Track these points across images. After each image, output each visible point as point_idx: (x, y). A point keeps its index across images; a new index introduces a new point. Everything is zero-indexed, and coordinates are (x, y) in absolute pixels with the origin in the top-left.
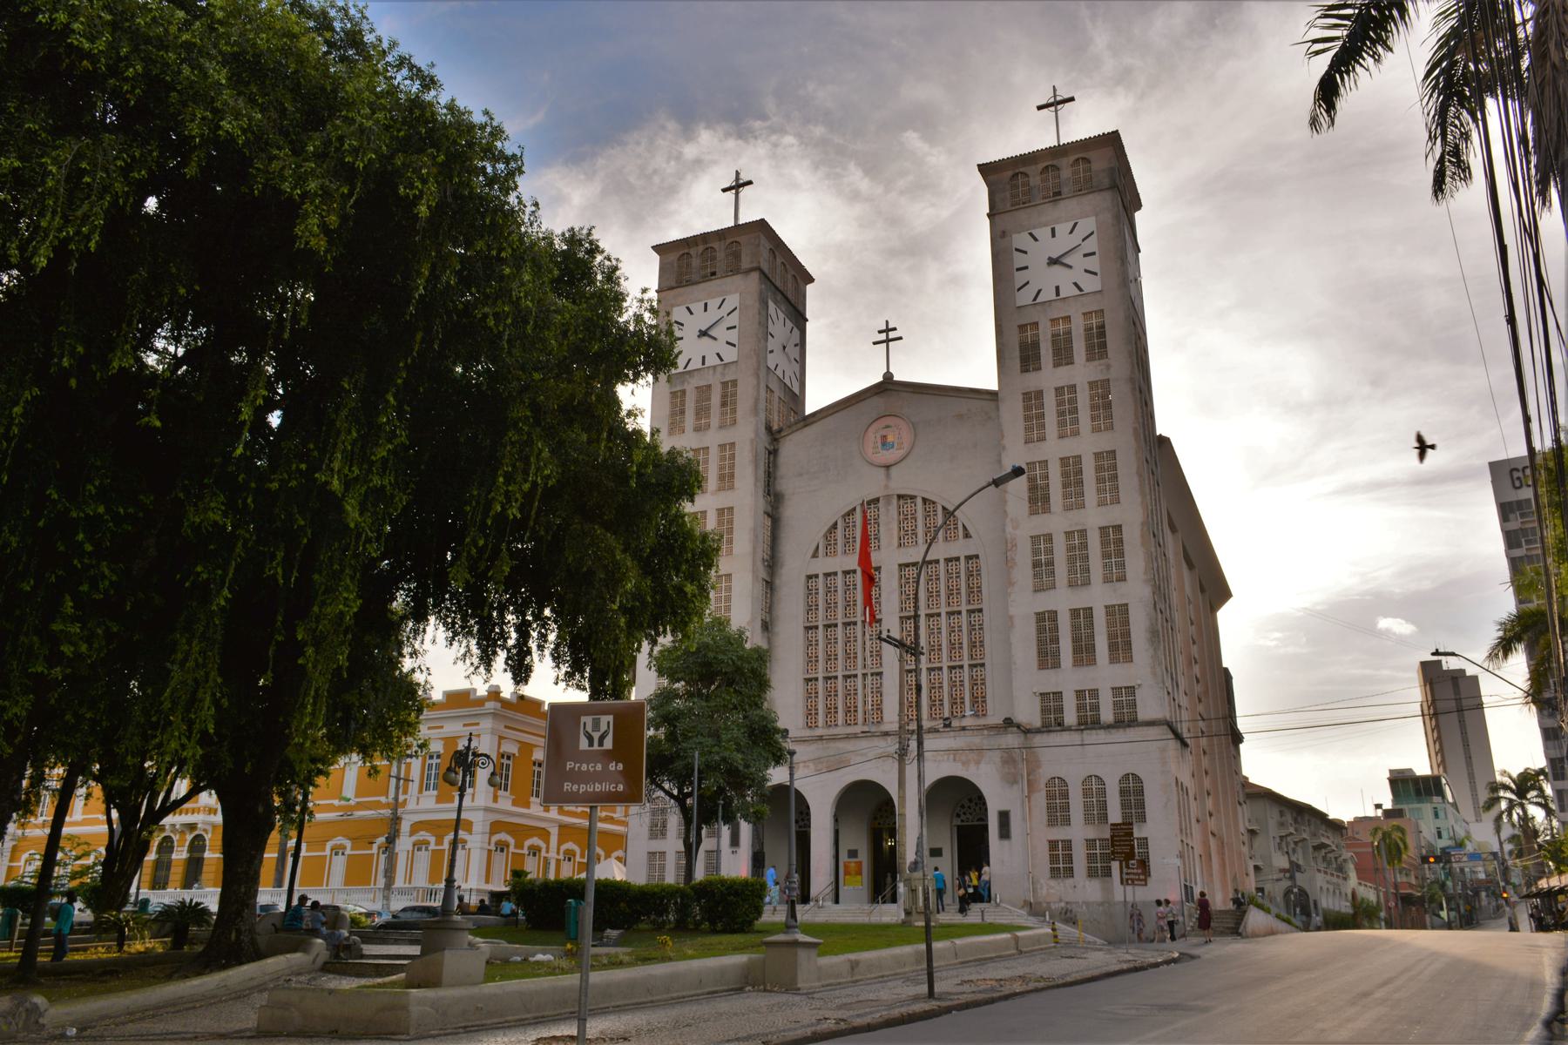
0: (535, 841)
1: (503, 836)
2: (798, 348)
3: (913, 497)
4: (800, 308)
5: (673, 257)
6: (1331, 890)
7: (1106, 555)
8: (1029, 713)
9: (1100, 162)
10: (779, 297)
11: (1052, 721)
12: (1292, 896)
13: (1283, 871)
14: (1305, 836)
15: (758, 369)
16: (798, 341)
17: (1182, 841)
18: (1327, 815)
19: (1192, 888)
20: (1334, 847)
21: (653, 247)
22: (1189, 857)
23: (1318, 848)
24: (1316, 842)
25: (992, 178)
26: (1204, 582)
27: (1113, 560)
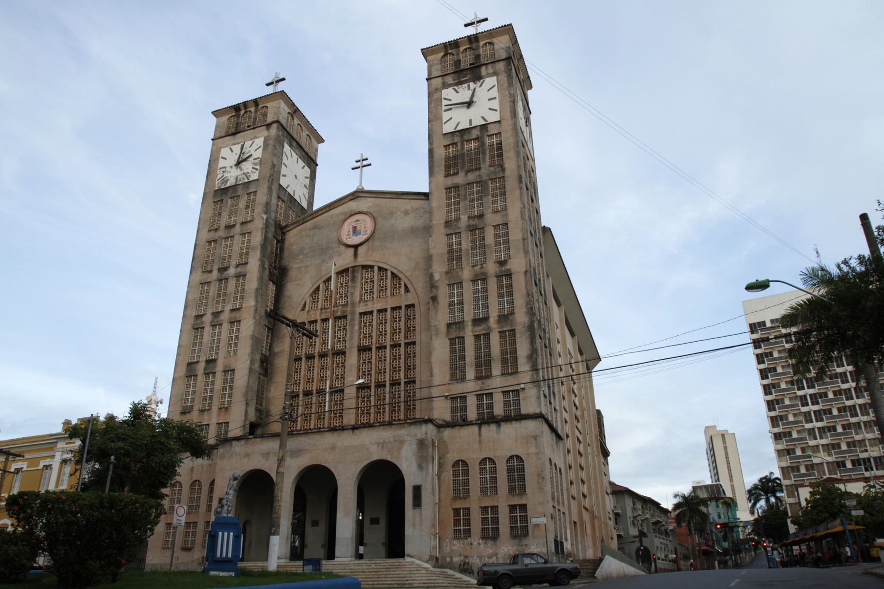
3: (372, 267)
6: (663, 548)
7: (501, 296)
8: (442, 410)
9: (501, 43)
11: (460, 422)
12: (640, 552)
13: (635, 537)
14: (648, 516)
15: (272, 184)
16: (309, 175)
17: (554, 507)
18: (660, 504)
19: (562, 543)
20: (664, 523)
22: (560, 520)
23: (655, 524)
24: (654, 520)
26: (568, 316)
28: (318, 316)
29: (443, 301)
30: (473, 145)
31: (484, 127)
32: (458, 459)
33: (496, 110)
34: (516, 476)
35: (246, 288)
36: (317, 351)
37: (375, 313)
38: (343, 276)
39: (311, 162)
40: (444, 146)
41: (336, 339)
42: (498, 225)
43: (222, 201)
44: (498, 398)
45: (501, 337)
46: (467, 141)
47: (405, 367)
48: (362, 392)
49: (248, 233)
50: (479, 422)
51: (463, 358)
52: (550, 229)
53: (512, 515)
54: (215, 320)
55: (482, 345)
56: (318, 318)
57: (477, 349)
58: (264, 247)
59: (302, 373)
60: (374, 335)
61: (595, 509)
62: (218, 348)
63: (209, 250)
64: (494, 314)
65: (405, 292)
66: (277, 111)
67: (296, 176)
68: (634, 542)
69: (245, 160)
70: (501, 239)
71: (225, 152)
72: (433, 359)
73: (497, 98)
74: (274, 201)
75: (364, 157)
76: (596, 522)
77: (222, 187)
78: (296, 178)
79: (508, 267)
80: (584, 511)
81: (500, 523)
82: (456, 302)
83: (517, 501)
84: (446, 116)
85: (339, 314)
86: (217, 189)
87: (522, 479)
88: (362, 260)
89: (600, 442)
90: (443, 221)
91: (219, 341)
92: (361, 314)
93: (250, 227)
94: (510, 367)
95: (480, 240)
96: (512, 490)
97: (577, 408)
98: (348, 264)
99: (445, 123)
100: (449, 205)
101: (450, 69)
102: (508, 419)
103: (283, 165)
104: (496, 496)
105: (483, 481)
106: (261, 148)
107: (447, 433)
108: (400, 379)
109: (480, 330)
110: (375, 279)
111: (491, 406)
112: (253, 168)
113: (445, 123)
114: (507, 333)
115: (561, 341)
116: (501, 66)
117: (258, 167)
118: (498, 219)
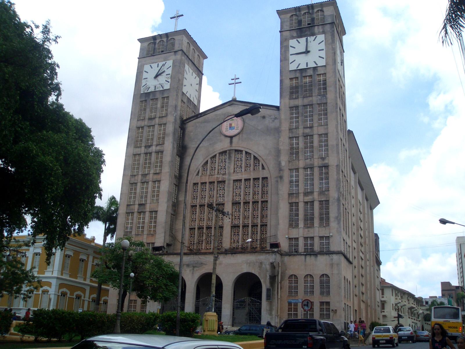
0: (79, 293)
1: (64, 290)
2: (198, 85)
3: (241, 151)
4: (200, 69)
5: (146, 44)
10: (190, 63)
11: (294, 252)
13: (395, 317)
16: (198, 83)
18: (415, 296)
21: (138, 40)
22: (348, 311)
25: (283, 16)
27: (324, 181)
28: (207, 179)
29: (286, 179)
30: (308, 80)
31: (315, 69)
32: (292, 274)
33: (323, 58)
34: (325, 286)
35: (163, 160)
36: (206, 201)
37: (243, 181)
38: (223, 155)
39: (200, 73)
40: (290, 79)
41: (218, 195)
42: (322, 134)
43: (146, 101)
44: (317, 241)
45: (320, 204)
46: (304, 77)
47: (261, 216)
48: (234, 229)
49: (164, 124)
50: (305, 254)
51: (297, 215)
52: (352, 132)
53: (321, 307)
54: (144, 179)
55: (309, 208)
56: (207, 181)
57: (306, 210)
58: (174, 133)
59: (197, 215)
60: (242, 194)
61: (369, 301)
62: (146, 197)
63: (138, 133)
64: (316, 189)
65: (262, 169)
66: (182, 43)
67: (191, 85)
68: (394, 321)
69: (160, 74)
70: (323, 143)
71: (147, 68)
72: (279, 215)
73: (324, 50)
74: (180, 103)
75: (237, 77)
76: (369, 309)
77: (146, 92)
78: (191, 85)
79: (326, 161)
80: (362, 303)
81: (314, 311)
82: (294, 180)
83: (325, 299)
84: (291, 58)
85: (220, 180)
86: (142, 92)
87: (328, 287)
88: (235, 146)
89: (376, 256)
90: (287, 129)
91: (147, 193)
92: (234, 180)
93: (164, 121)
94: (324, 222)
95: (310, 143)
96: (322, 293)
97: (362, 238)
98: (227, 148)
99: (291, 63)
100: (291, 118)
101: (295, 26)
102: (321, 253)
103: (184, 79)
104: (313, 296)
105: (306, 287)
106: (171, 68)
107: (286, 259)
108: (258, 223)
109: (308, 199)
110: (243, 159)
111: (312, 245)
112: (166, 81)
113: (291, 63)
114: (324, 202)
115: (354, 197)
116: (328, 28)
117: (169, 80)
118: (322, 131)
